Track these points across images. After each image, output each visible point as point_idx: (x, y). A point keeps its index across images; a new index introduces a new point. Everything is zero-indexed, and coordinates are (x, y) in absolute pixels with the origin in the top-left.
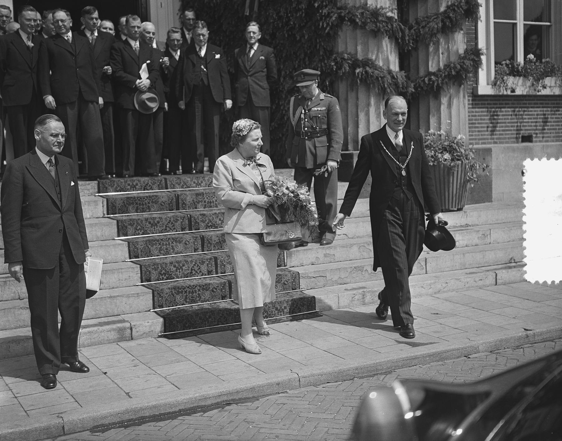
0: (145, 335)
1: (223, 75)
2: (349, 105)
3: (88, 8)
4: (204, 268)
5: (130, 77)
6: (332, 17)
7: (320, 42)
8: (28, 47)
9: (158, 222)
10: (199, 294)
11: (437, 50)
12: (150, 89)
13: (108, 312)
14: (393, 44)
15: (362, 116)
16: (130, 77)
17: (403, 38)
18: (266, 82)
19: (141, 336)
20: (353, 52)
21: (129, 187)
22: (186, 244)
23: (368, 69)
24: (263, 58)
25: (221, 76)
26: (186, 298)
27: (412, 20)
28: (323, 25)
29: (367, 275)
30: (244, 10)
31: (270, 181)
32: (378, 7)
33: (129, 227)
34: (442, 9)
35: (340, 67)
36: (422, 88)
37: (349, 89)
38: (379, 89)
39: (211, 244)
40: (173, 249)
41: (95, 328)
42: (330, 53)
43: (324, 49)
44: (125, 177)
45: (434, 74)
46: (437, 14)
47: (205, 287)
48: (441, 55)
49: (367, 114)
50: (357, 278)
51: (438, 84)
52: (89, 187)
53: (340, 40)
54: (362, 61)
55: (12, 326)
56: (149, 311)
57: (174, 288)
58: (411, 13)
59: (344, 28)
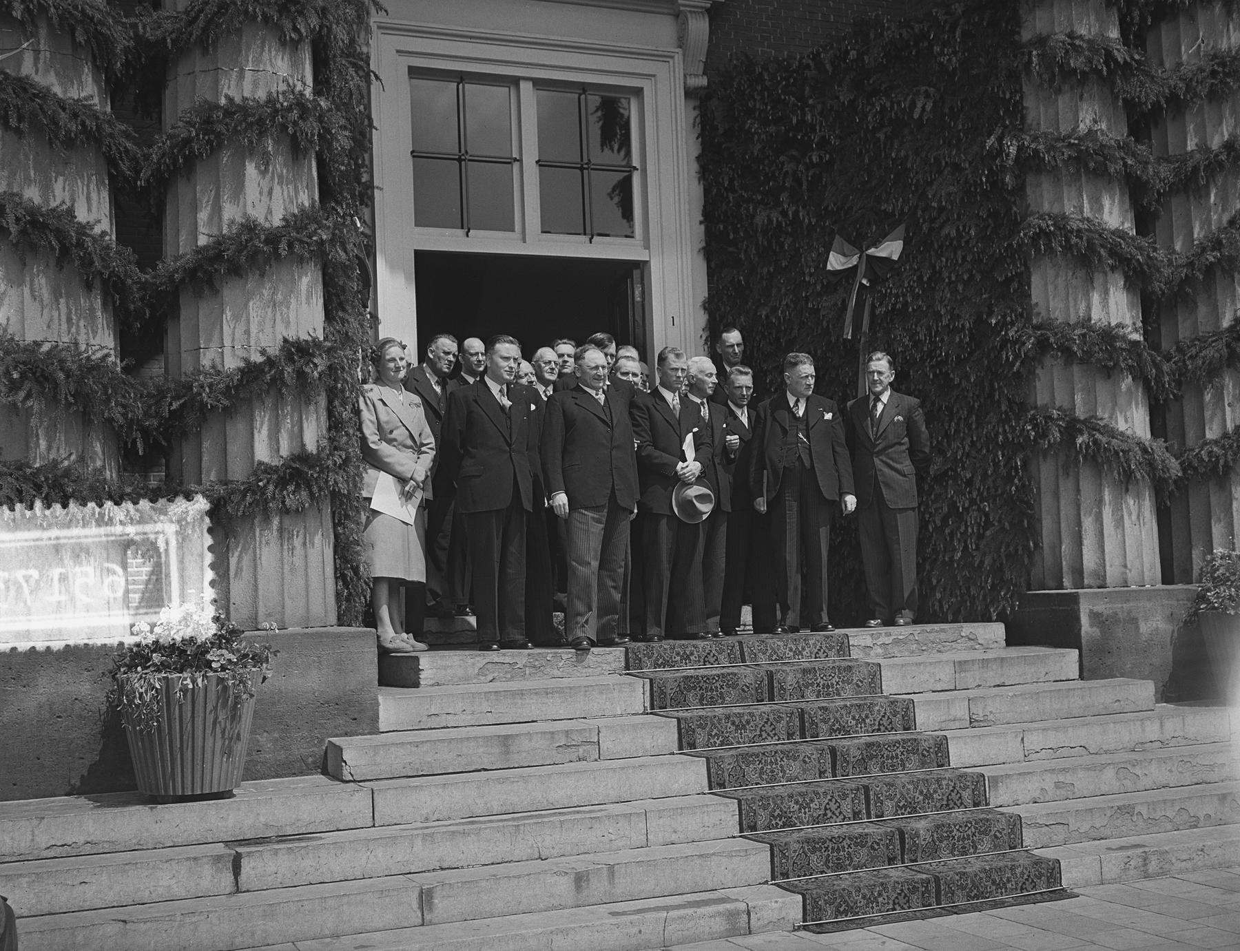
0: (770, 927)
1: (838, 449)
2: (1062, 502)
3: (599, 336)
4: (847, 807)
5: (666, 458)
6: (1024, 343)
7: (1000, 387)
8: (502, 408)
9: (748, 722)
10: (849, 853)
11: (1219, 397)
12: (700, 480)
13: (696, 883)
14: (1140, 389)
15: (1088, 523)
16: (666, 458)
17: (1158, 379)
18: (908, 462)
19: (764, 929)
20: (1066, 405)
21: (678, 658)
22: (804, 762)
23: (1098, 436)
24: (900, 418)
25: (834, 451)
26: (827, 860)
27: (1166, 345)
28: (1007, 358)
29: (1140, 822)
30: (842, 329)
31: (99, 128)
32: (1113, 324)
33: (698, 730)
34: (1226, 323)
35: (1043, 434)
36: (1195, 469)
37: (1061, 472)
38: (1119, 473)
39: (848, 763)
40: (783, 771)
41: (690, 911)
42: (1021, 408)
43: (1009, 399)
44: (651, 640)
45: (1216, 442)
46: (1218, 334)
47: (860, 840)
48: (1228, 409)
49: (1099, 519)
50: (1124, 829)
51: (1226, 462)
52: (610, 658)
53: (1038, 384)
54: (1084, 422)
55: (541, 906)
56: (766, 882)
57: (807, 841)
58: (1163, 330)
59: (1048, 361)
